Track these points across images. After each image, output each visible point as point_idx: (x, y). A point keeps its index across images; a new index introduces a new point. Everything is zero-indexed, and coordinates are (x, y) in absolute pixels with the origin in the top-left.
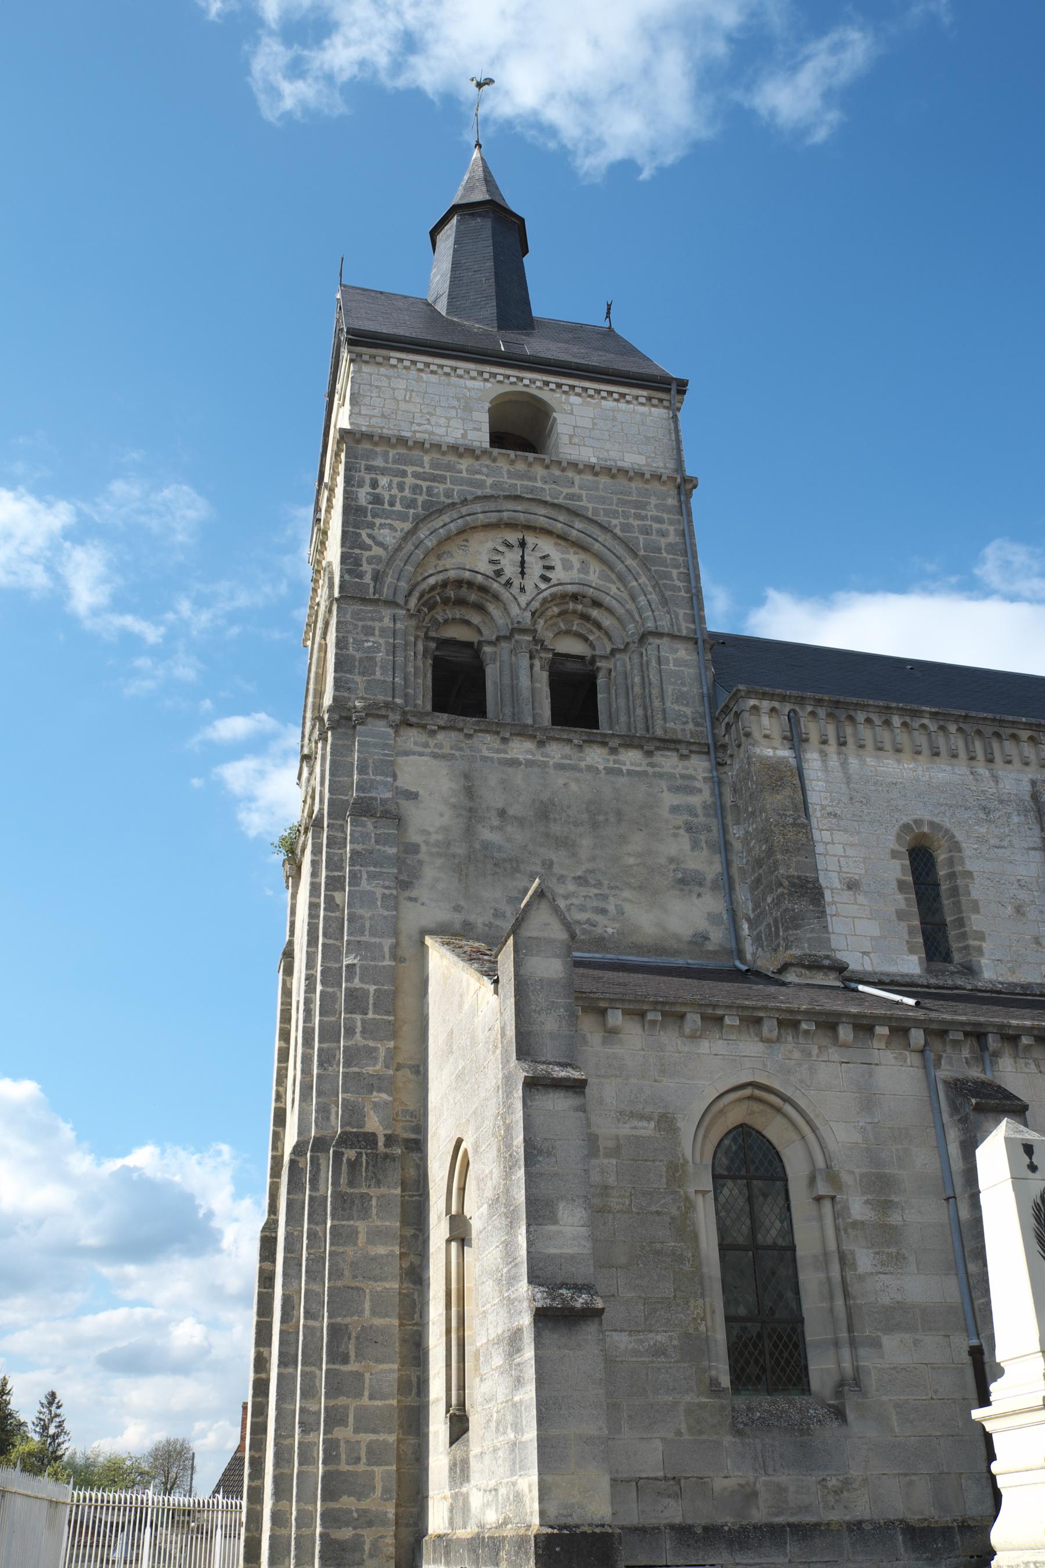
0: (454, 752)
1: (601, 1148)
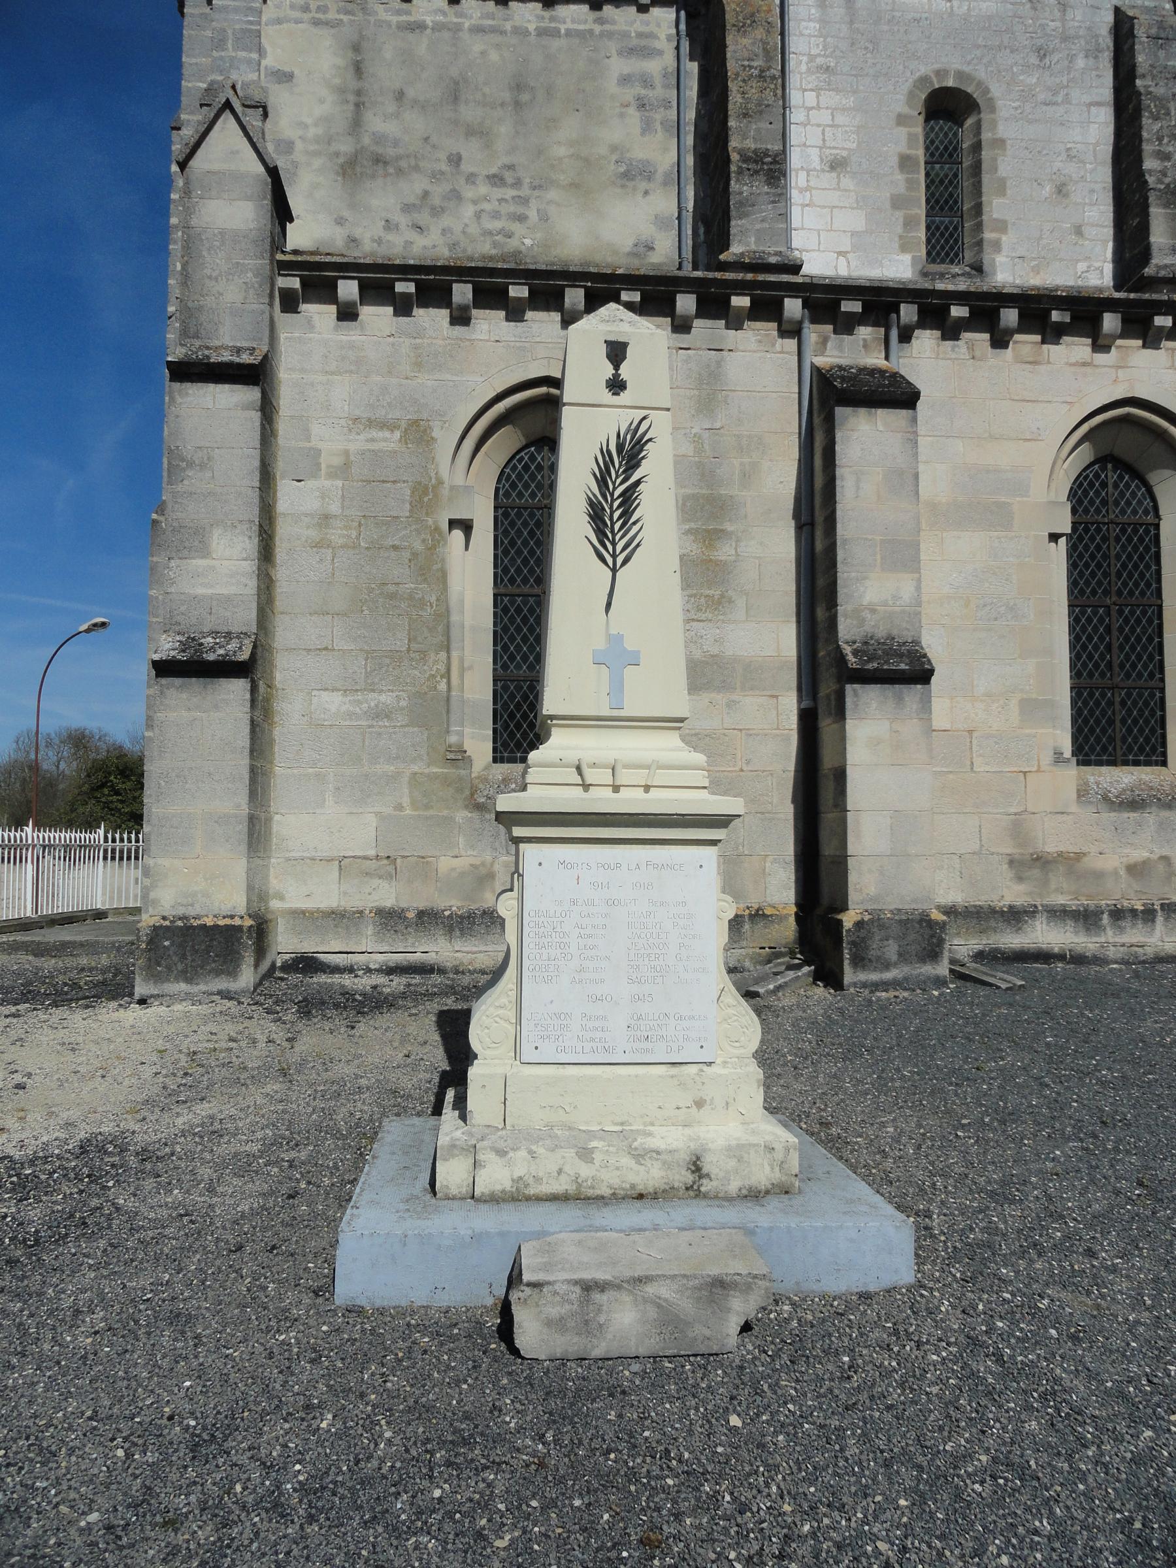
0: (341, 16)
1: (323, 466)
